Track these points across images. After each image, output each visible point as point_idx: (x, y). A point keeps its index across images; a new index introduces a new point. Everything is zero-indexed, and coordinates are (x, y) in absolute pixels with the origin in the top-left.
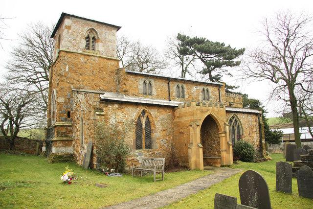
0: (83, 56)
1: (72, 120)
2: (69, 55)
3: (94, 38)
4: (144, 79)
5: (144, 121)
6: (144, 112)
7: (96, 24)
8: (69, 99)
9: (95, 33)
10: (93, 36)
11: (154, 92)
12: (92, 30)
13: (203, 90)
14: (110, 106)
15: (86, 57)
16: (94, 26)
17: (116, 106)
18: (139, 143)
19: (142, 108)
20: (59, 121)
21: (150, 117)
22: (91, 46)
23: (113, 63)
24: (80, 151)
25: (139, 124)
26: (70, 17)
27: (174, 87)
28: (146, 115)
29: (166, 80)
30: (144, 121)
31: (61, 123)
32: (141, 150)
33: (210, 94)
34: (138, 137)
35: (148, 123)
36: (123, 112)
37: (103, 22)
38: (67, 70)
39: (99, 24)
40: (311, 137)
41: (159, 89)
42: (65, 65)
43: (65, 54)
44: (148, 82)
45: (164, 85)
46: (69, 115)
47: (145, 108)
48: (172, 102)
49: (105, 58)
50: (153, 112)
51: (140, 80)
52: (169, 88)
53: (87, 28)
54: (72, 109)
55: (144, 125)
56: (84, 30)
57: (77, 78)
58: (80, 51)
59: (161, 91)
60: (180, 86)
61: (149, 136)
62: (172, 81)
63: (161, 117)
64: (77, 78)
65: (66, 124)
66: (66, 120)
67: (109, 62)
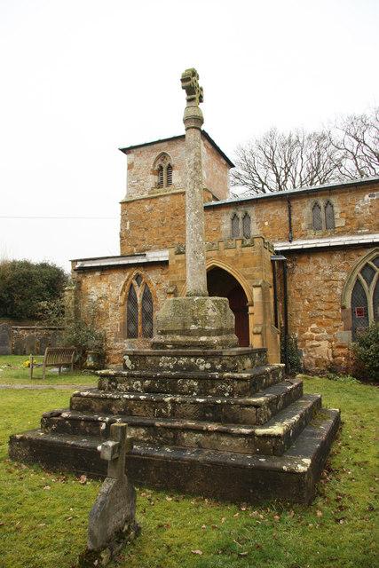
4: (232, 211)
5: (139, 292)
6: (138, 277)
7: (166, 144)
11: (340, 223)
14: (89, 276)
16: (164, 148)
17: (98, 274)
18: (132, 328)
19: (135, 272)
25: (131, 298)
27: (304, 211)
29: (282, 200)
30: (139, 292)
32: (133, 340)
34: (131, 318)
35: (147, 296)
36: (329, 262)
37: (128, 146)
38: (128, 228)
41: (266, 224)
44: (240, 215)
45: (280, 212)
48: (294, 243)
52: (290, 216)
57: (140, 237)
59: (272, 225)
61: (148, 316)
62: (294, 199)
64: (140, 237)
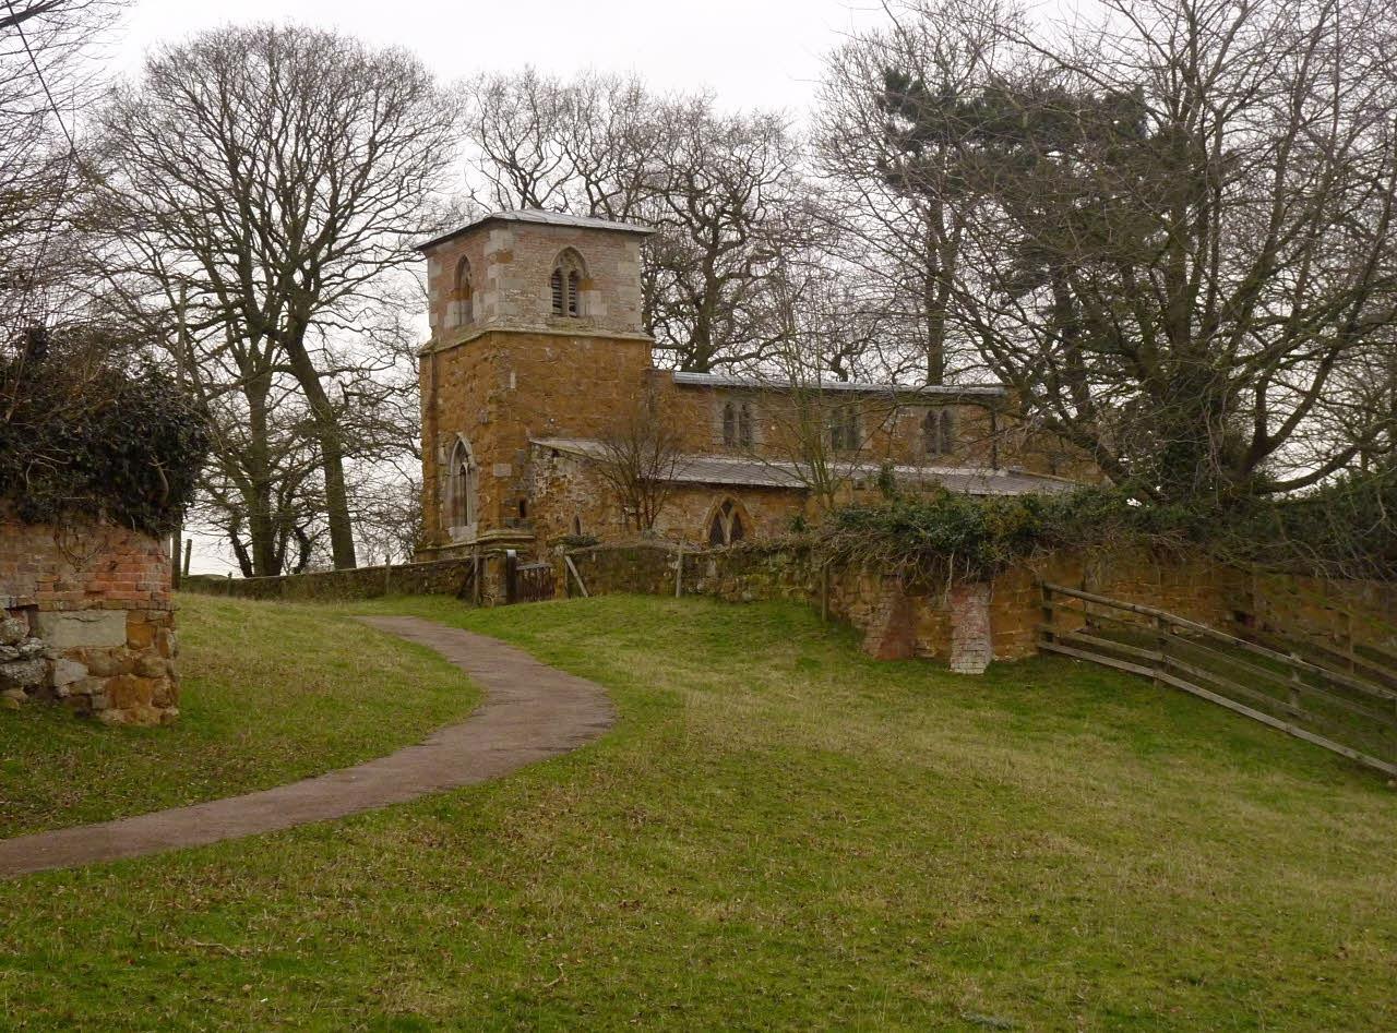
0: (551, 341)
1: (530, 525)
2: (514, 342)
3: (574, 276)
4: (725, 399)
6: (727, 505)
7: (580, 232)
8: (522, 467)
9: (576, 261)
10: (571, 269)
12: (569, 253)
13: (931, 416)
15: (559, 341)
20: (501, 527)
21: (743, 518)
22: (567, 303)
23: (633, 351)
24: (881, 606)
26: (510, 225)
28: (733, 511)
31: (507, 531)
33: (956, 431)
39: (459, 239)
40: (238, 575)
42: (509, 371)
43: (504, 338)
46: (523, 513)
47: (729, 495)
49: (610, 339)
50: (751, 505)
51: (716, 406)
53: (555, 250)
54: (531, 494)
55: (729, 535)
56: (547, 259)
58: (541, 327)
60: (738, 408)
63: (772, 515)
65: (517, 533)
66: (516, 524)
67: (622, 350)
